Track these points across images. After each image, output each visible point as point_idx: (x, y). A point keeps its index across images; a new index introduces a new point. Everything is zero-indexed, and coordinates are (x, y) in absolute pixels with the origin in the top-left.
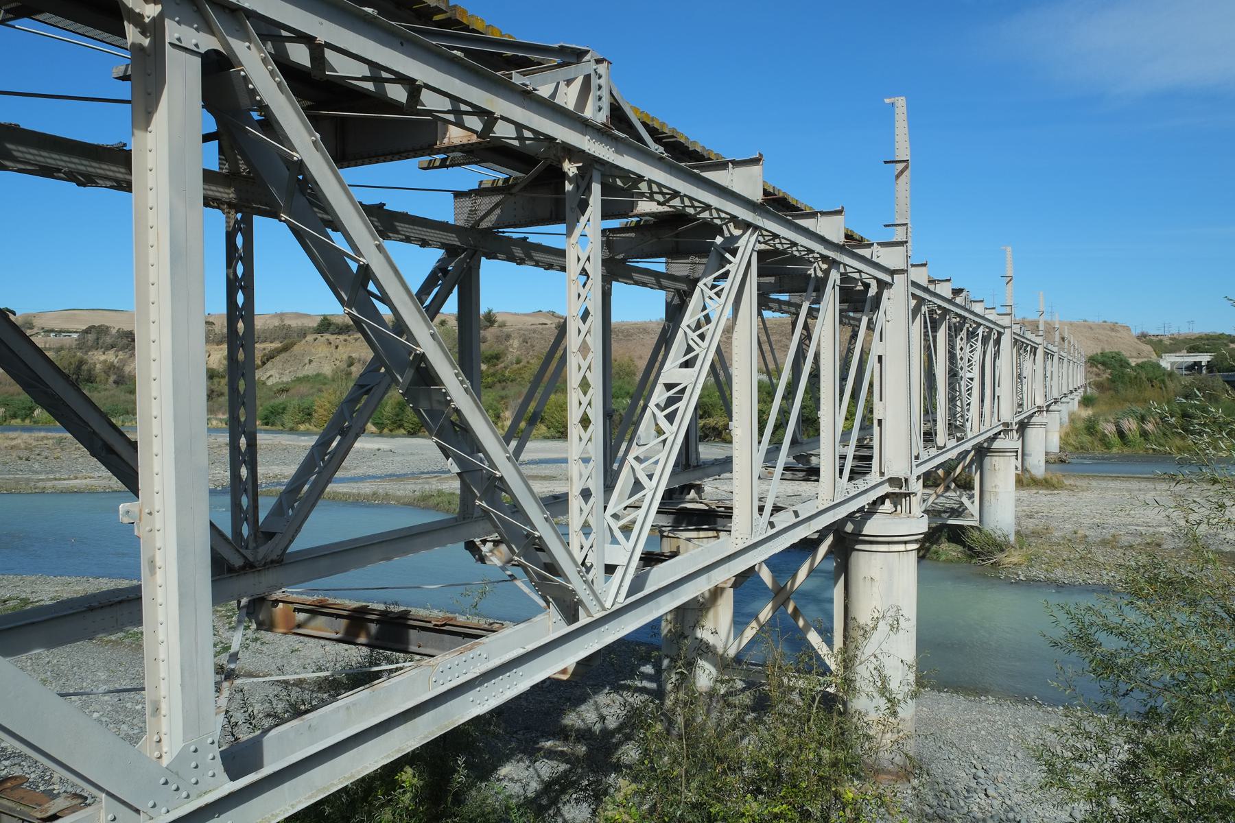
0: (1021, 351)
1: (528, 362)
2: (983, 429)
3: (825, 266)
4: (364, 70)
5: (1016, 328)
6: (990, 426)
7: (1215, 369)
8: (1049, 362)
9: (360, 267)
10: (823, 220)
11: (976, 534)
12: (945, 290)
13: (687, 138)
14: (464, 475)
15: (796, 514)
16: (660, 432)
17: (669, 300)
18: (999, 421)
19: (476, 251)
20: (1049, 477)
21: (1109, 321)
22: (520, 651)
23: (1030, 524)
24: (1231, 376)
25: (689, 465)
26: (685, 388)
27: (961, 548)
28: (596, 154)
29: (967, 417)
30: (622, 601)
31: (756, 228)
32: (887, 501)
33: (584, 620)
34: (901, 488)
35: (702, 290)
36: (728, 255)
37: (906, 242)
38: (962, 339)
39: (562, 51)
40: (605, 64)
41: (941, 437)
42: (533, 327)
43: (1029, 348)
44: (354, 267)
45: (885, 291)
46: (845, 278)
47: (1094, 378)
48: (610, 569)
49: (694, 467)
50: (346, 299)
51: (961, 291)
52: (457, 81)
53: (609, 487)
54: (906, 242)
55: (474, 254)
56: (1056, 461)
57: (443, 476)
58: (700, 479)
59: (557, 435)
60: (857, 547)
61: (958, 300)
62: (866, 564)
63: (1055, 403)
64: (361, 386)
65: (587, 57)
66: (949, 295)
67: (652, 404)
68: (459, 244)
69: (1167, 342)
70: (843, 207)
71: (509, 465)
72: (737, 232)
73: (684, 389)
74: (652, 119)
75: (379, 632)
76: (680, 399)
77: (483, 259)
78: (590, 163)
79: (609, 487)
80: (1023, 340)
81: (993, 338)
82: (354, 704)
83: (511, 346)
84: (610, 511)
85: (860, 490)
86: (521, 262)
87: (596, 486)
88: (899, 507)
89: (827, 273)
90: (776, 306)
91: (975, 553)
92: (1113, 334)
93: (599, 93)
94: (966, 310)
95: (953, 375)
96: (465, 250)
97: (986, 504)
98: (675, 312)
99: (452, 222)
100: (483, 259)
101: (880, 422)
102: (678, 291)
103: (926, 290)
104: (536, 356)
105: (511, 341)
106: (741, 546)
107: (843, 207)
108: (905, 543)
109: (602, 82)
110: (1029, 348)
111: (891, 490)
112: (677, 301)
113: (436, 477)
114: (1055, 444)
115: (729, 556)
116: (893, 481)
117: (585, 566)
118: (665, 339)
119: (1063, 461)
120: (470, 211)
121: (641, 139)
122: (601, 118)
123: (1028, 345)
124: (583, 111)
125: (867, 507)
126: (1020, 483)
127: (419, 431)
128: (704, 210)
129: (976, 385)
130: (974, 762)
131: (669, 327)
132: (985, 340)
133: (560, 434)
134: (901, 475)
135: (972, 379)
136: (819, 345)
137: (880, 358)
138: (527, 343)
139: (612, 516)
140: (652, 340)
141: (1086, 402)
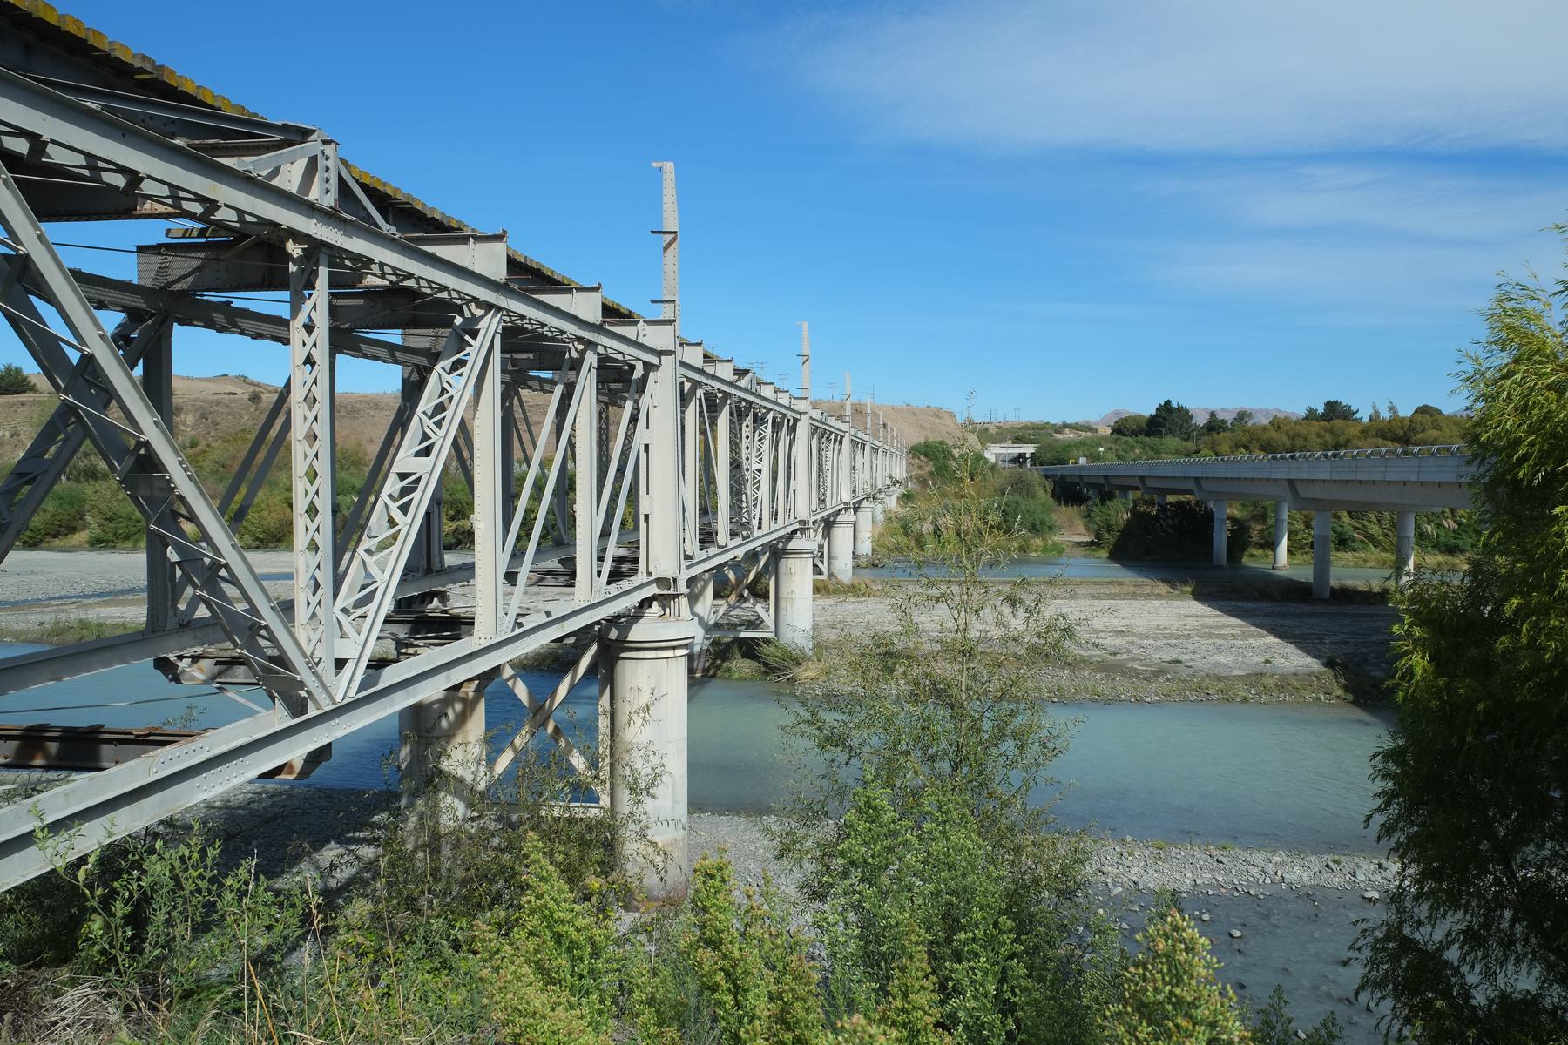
0: (824, 440)
1: (208, 446)
2: (774, 527)
3: (580, 347)
4: (81, 160)
5: (816, 414)
6: (785, 525)
7: (1038, 461)
9: (83, 357)
10: (578, 297)
11: (771, 649)
12: (725, 372)
13: (424, 204)
14: (185, 565)
15: (548, 614)
16: (392, 523)
17: (406, 376)
19: (167, 317)
20: (856, 583)
21: (933, 406)
22: (248, 740)
23: (831, 635)
24: (1050, 469)
25: (431, 570)
26: (420, 478)
27: (755, 664)
28: (324, 239)
29: (753, 513)
30: (353, 695)
31: (499, 309)
32: (655, 603)
33: (312, 712)
34: (669, 589)
35: (421, 420)
36: (467, 338)
37: (675, 321)
38: (747, 426)
39: (286, 128)
40: (333, 145)
41: (723, 536)
42: (216, 397)
43: (832, 437)
44: (74, 357)
45: (651, 373)
46: (604, 360)
47: (916, 471)
48: (340, 664)
49: (437, 572)
50: (63, 386)
51: (746, 372)
52: (179, 170)
53: (338, 581)
54: (675, 321)
55: (164, 321)
56: (868, 565)
57: (85, 601)
58: (443, 586)
59: (254, 544)
60: (623, 655)
61: (744, 383)
62: (636, 675)
64: (21, 475)
65: (314, 137)
66: (730, 377)
67: (384, 495)
68: (144, 305)
69: (993, 430)
70: (600, 284)
71: (234, 553)
72: (479, 312)
73: (419, 479)
74: (385, 184)
75: (60, 751)
76: (414, 489)
77: (175, 324)
78: (316, 249)
79: (338, 581)
80: (825, 427)
81: (785, 425)
82: (73, 791)
83: (183, 422)
84: (340, 603)
85: (621, 591)
86: (221, 329)
87: (326, 577)
88: (668, 610)
89: (582, 354)
90: (535, 384)
91: (770, 668)
92: (938, 420)
93: (326, 175)
94: (752, 394)
96: (153, 315)
97: (782, 613)
98: (412, 390)
99: (135, 282)
100: (175, 324)
101: (647, 516)
102: (417, 366)
103: (701, 372)
104: (221, 437)
105: (183, 417)
106: (485, 644)
107: (600, 284)
108: (674, 648)
109: (330, 163)
110: (832, 437)
111: (658, 591)
112: (415, 377)
113: (74, 603)
115: (471, 654)
116: (661, 582)
117: (313, 664)
118: (401, 422)
119: (875, 566)
120: (160, 268)
121: (368, 218)
122: (329, 201)
123: (831, 433)
124: (307, 193)
125: (633, 611)
126: (818, 589)
127: (41, 541)
128: (440, 291)
129: (765, 478)
130: (749, 880)
131: (405, 406)
133: (258, 543)
134: (669, 575)
135: (760, 471)
136: (573, 429)
137: (647, 447)
138: (207, 419)
139: (366, 551)
140: (386, 420)
141: (906, 498)
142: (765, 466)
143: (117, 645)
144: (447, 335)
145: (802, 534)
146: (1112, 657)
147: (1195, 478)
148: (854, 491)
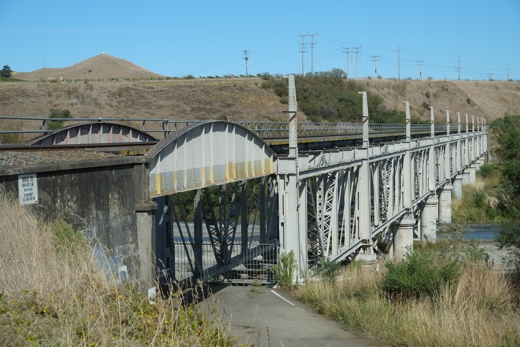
8: (454, 148)
18: (403, 207)
63: (467, 168)
88: (366, 251)
95: (381, 190)
101: (403, 192)
111: (363, 244)
114: (447, 216)
129: (391, 191)
132: (395, 165)
134: (367, 239)
135: (389, 188)
142: (334, 214)
143: (394, 202)
144: (184, 224)
145: (364, 250)
148: (451, 171)
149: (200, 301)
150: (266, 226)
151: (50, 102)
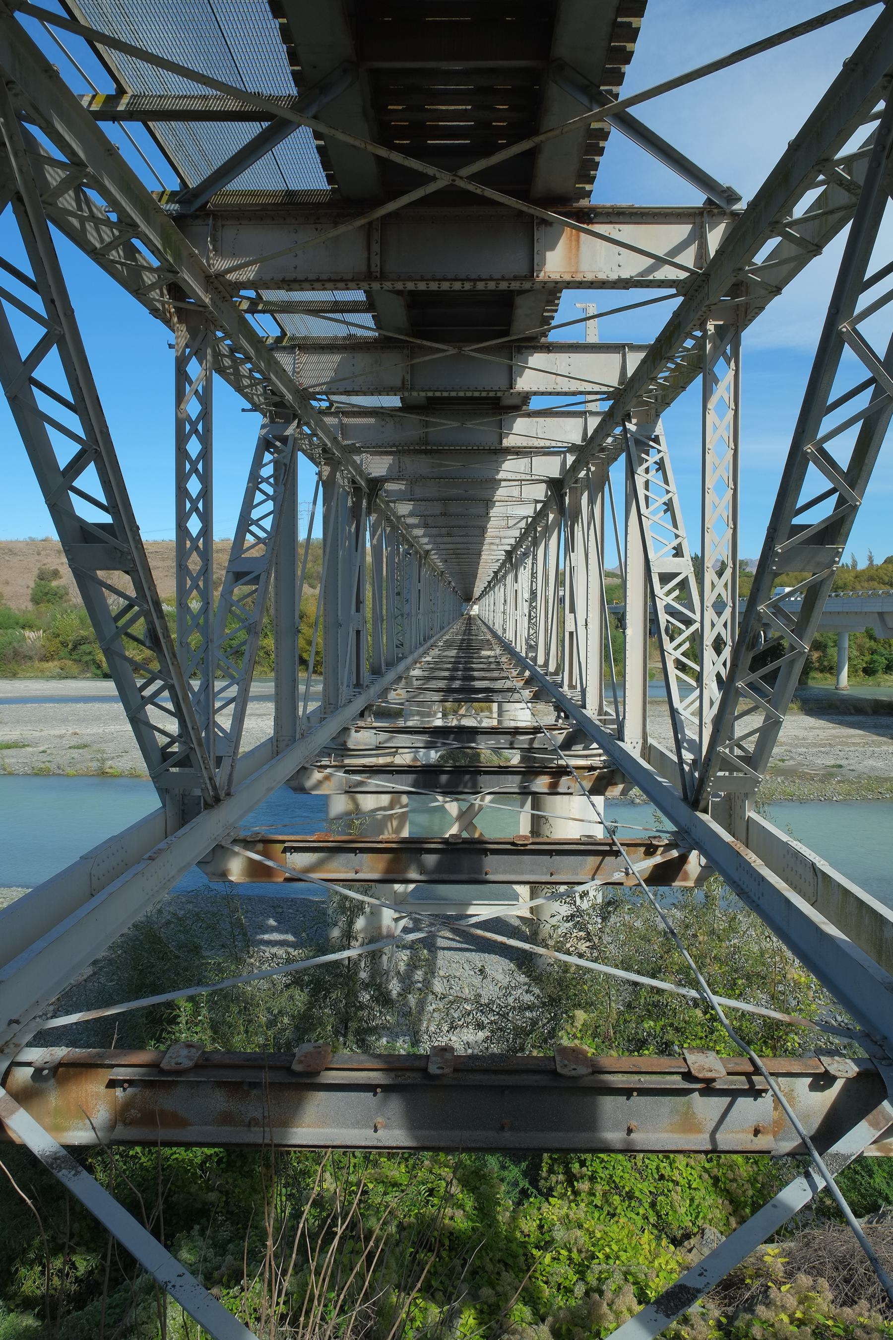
36: (643, 455)
146: (781, 763)
147: (878, 613)
149: (735, 194)
150: (368, 533)
151: (38, 561)
